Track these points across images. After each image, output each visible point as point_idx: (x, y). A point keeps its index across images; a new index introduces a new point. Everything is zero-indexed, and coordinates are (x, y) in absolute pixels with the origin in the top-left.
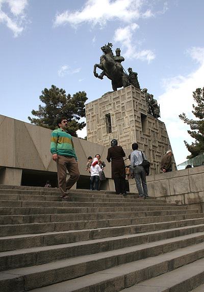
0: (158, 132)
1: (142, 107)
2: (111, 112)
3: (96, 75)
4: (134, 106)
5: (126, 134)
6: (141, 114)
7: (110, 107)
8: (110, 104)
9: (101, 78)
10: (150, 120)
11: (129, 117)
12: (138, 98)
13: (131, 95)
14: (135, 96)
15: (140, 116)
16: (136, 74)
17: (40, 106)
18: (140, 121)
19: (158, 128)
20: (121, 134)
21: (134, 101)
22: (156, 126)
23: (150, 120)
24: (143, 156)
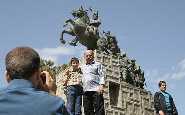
1: (112, 74)
3: (64, 42)
6: (110, 82)
9: (74, 45)
15: (108, 84)
16: (114, 38)
19: (139, 99)
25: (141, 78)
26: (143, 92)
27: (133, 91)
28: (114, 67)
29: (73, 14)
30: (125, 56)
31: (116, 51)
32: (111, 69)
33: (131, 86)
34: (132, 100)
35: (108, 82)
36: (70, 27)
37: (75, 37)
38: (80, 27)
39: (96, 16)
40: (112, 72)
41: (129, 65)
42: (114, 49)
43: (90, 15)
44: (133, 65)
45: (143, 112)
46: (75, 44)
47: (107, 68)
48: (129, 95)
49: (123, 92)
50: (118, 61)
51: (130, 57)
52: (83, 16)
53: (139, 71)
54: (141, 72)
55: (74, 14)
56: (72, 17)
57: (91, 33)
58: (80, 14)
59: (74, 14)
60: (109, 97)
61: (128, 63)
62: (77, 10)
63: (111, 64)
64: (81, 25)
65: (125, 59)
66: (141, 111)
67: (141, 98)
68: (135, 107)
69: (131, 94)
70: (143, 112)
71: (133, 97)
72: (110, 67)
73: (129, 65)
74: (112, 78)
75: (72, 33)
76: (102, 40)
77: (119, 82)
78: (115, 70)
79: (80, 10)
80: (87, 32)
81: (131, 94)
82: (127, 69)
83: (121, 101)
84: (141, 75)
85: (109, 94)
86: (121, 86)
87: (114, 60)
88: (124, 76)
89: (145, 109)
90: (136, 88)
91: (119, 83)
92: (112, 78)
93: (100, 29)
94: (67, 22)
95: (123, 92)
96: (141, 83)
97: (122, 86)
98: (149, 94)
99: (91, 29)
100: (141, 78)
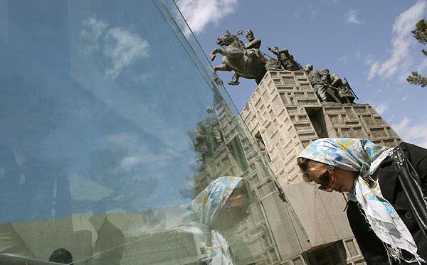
0: (360, 124)
1: (306, 97)
2: (260, 128)
4: (284, 102)
5: (291, 154)
7: (256, 121)
8: (255, 117)
9: (236, 83)
10: (332, 112)
11: (284, 124)
12: (290, 86)
13: (274, 86)
14: (282, 83)
15: (305, 113)
16: (286, 53)
17: (230, 84)
18: (308, 120)
19: (357, 119)
20: (284, 159)
21: (282, 94)
22: (351, 117)
23: (332, 112)
24: (280, 114)
25: (346, 89)
26: (357, 108)
27: (343, 111)
28: (304, 87)
29: (219, 43)
30: (311, 69)
31: (296, 67)
32: (300, 90)
33: (337, 105)
34: (348, 123)
35: (304, 109)
36: (222, 60)
37: (233, 72)
38: (233, 54)
39: (251, 35)
40: (303, 93)
41: (323, 78)
42: (292, 67)
43: (242, 38)
44: (328, 76)
45: (369, 135)
46: (237, 81)
47: (295, 90)
48: (340, 117)
49: (331, 116)
50: (305, 76)
51: (321, 70)
52: (234, 40)
53: (339, 81)
54: (344, 82)
55: (221, 43)
56: (219, 47)
57: (253, 56)
58: (228, 41)
59: (221, 43)
60: (313, 129)
61: (321, 76)
62: (223, 37)
63: (298, 83)
64: (235, 52)
65: (313, 72)
66: (366, 135)
67: (359, 116)
68: (356, 132)
69: (343, 116)
70: (369, 135)
71: (348, 119)
72: (298, 88)
73: (323, 78)
74: (307, 101)
75: (228, 68)
76: (271, 61)
77: (319, 104)
78: (306, 90)
79: (226, 36)
80: (246, 58)
81: (343, 116)
82: (322, 84)
83: (334, 130)
84: (345, 85)
85: (311, 125)
86: (344, 242)
87: (300, 77)
88: (322, 95)
89: (371, 130)
90: (346, 105)
91: (320, 105)
92: (307, 101)
93: (263, 49)
94: (214, 53)
95: (331, 116)
96: (349, 97)
97: (326, 109)
98: (367, 108)
99: (250, 52)
100: (346, 89)
